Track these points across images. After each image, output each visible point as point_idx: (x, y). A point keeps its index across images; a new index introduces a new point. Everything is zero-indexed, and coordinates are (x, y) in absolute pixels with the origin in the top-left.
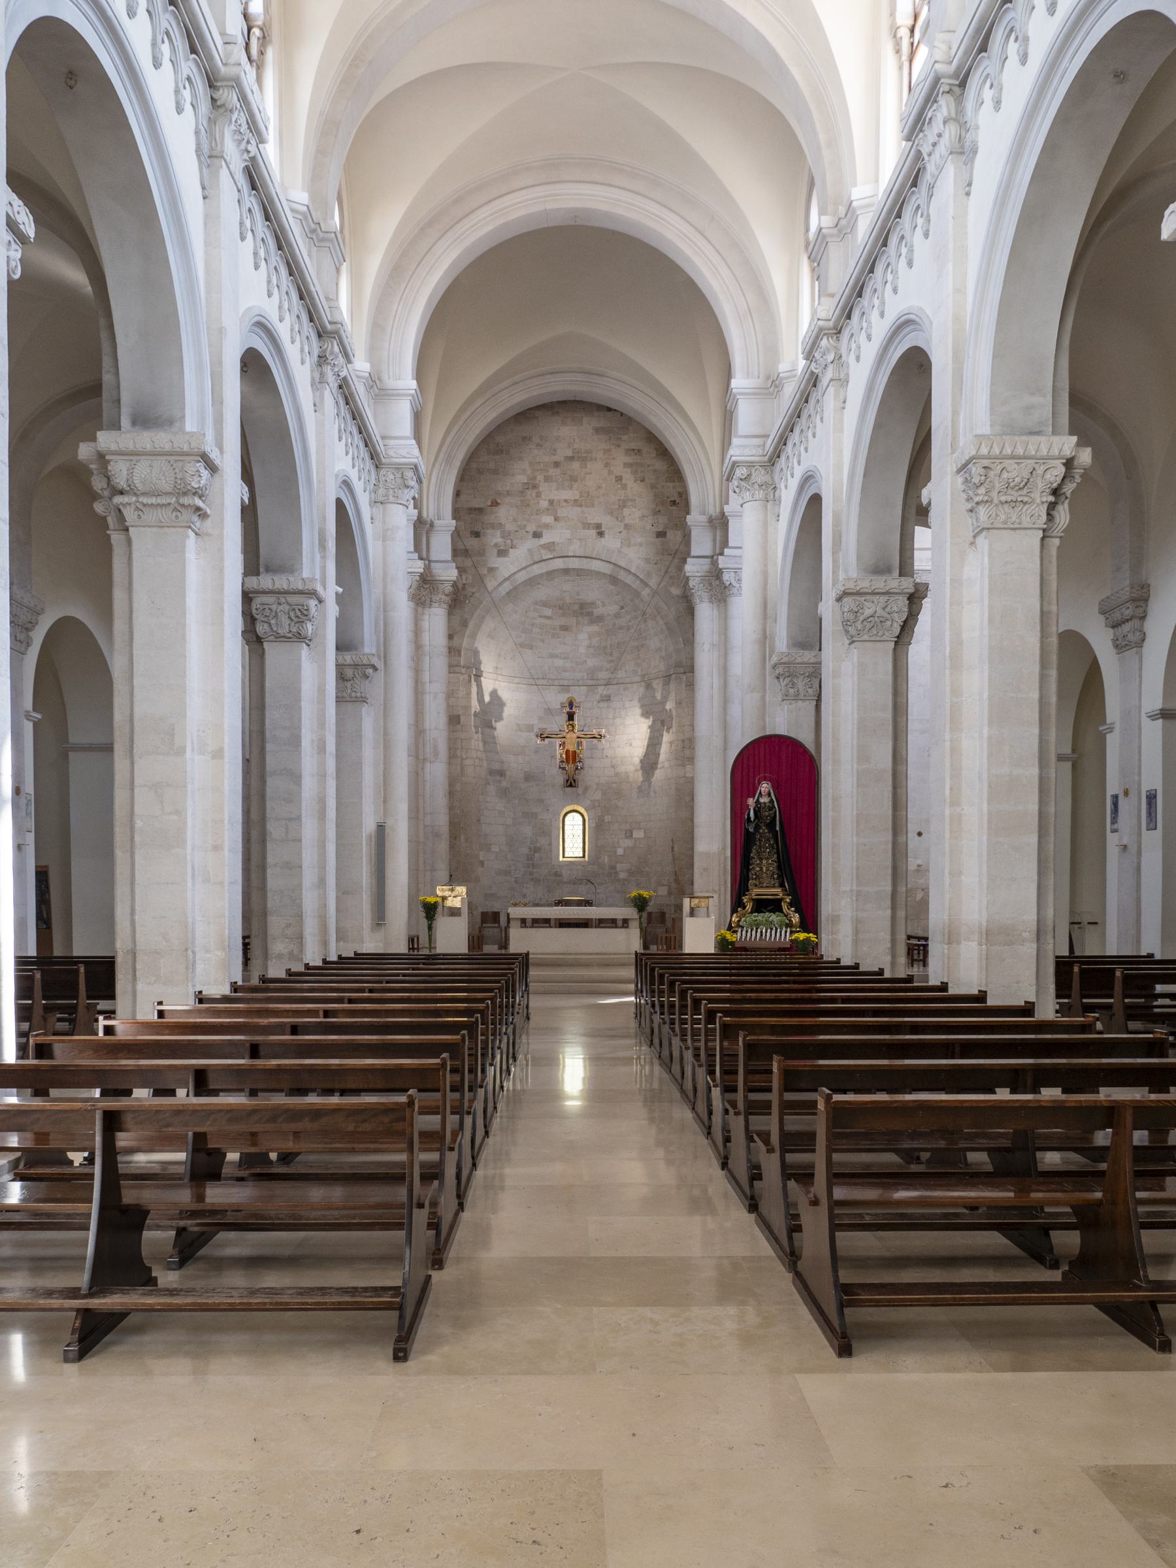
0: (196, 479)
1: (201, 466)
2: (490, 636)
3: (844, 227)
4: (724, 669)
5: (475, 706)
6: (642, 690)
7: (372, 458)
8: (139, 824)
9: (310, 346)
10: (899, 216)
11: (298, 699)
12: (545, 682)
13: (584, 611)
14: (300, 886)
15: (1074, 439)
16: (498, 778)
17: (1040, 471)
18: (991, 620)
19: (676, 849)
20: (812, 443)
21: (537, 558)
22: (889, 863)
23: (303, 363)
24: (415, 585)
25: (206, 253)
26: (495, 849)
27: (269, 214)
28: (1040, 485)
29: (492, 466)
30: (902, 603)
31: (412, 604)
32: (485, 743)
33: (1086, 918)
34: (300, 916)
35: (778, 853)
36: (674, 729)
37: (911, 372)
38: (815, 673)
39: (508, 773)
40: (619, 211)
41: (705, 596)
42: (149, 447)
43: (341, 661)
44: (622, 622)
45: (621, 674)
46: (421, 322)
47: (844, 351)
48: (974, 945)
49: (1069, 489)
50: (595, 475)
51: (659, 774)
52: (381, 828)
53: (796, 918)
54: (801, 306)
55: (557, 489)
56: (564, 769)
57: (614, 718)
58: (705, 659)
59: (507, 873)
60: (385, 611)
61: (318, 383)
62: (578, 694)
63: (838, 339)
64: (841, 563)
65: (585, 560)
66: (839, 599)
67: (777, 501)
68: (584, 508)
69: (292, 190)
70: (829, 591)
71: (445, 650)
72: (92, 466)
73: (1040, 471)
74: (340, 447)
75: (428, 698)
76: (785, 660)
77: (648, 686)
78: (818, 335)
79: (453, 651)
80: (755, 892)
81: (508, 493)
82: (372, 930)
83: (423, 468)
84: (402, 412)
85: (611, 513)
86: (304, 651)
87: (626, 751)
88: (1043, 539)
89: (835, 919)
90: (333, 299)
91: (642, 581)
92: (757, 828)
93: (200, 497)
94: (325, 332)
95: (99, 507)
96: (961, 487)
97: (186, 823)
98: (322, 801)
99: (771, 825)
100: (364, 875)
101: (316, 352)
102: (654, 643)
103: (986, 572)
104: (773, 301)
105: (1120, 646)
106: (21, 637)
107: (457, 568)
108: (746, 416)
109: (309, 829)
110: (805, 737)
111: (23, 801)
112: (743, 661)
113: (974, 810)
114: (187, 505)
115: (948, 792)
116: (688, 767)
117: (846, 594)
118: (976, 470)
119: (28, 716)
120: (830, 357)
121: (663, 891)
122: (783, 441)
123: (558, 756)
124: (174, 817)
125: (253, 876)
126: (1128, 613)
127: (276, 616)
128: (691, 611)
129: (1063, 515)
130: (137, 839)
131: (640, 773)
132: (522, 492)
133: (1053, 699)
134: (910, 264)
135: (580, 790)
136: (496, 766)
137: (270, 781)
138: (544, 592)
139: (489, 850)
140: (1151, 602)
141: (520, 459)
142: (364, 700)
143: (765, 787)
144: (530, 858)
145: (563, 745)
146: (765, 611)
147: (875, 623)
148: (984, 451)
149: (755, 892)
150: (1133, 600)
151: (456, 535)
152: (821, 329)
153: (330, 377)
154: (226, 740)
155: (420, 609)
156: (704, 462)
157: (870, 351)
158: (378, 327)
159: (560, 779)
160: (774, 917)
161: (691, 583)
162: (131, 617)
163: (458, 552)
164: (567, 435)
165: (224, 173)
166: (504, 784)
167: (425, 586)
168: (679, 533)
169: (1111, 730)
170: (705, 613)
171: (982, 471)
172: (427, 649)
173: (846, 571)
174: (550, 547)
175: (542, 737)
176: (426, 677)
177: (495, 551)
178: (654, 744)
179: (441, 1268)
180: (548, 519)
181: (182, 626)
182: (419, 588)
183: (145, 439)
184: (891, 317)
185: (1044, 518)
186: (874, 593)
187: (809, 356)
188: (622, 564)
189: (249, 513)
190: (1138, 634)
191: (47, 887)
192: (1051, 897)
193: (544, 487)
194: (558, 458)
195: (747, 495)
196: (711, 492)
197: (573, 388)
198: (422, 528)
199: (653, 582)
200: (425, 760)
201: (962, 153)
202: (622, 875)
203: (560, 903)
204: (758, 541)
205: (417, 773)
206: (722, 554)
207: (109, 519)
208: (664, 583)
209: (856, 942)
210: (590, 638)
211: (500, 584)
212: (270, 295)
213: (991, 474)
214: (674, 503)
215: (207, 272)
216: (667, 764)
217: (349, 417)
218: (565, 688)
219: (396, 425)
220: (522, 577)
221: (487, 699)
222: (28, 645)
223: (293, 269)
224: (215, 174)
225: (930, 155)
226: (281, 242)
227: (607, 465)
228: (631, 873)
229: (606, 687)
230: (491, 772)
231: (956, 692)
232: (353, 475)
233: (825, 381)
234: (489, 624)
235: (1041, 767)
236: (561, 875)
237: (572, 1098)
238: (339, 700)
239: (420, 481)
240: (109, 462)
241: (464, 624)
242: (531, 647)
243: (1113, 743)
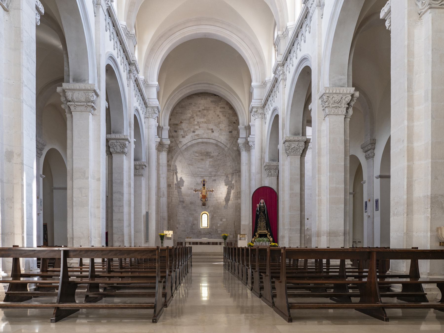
0: (92, 98)
1: (94, 94)
3: (285, 35)
4: (250, 171)
5: (175, 182)
6: (225, 178)
7: (146, 101)
8: (74, 199)
9: (126, 67)
10: (301, 28)
11: (123, 171)
12: (196, 175)
13: (208, 154)
14: (123, 226)
15: (354, 88)
17: (344, 98)
18: (330, 141)
20: (276, 99)
22: (299, 220)
23: (124, 72)
24: (157, 145)
25: (96, 32)
26: (181, 224)
27: (114, 25)
28: (344, 102)
29: (180, 112)
30: (303, 144)
31: (156, 151)
32: (178, 193)
33: (357, 241)
34: (123, 235)
36: (235, 189)
37: (306, 74)
38: (277, 169)
40: (219, 34)
41: (244, 149)
42: (78, 88)
43: (135, 164)
44: (219, 158)
45: (219, 173)
46: (160, 65)
47: (285, 71)
48: (325, 237)
49: (352, 104)
50: (211, 114)
51: (230, 202)
52: (147, 213)
53: (271, 239)
54: (272, 59)
58: (244, 168)
59: (185, 231)
61: (129, 78)
62: (206, 179)
63: (283, 67)
64: (285, 132)
66: (284, 143)
67: (265, 118)
69: (122, 22)
70: (281, 141)
71: (166, 165)
72: (61, 94)
73: (344, 98)
74: (135, 99)
75: (161, 179)
76: (268, 164)
77: (227, 177)
78: (278, 66)
79: (169, 166)
80: (259, 232)
81: (185, 120)
83: (160, 108)
84: (154, 92)
85: (216, 126)
86: (125, 157)
87: (221, 196)
88: (345, 118)
89: (283, 237)
90: (133, 54)
92: (260, 213)
93: (94, 103)
94: (131, 63)
95: (63, 106)
96: (320, 103)
97: (89, 199)
98: (130, 201)
100: (142, 227)
101: (128, 69)
102: (229, 164)
103: (328, 127)
104: (264, 59)
105: (367, 158)
106: (39, 152)
108: (256, 93)
109: (126, 209)
110: (274, 187)
111: (39, 202)
112: (255, 168)
113: (325, 197)
114: (90, 106)
115: (317, 192)
116: (239, 200)
117: (286, 141)
118: (325, 97)
119: (41, 176)
120: (281, 72)
122: (267, 100)
124: (85, 198)
125: (109, 223)
126: (369, 148)
127: (116, 146)
128: (239, 154)
129: (351, 111)
130: (74, 204)
133: (348, 165)
134: (305, 42)
135: (207, 207)
136: (182, 200)
137: (114, 195)
138: (196, 149)
139: (179, 224)
140: (376, 144)
141: (189, 109)
142: (142, 175)
143: (262, 201)
144: (192, 227)
146: (262, 150)
147: (295, 150)
148: (327, 92)
149: (259, 232)
150: (371, 144)
151: (170, 131)
152: (278, 64)
153: (132, 77)
154: (101, 175)
156: (244, 111)
157: (293, 69)
158: (146, 66)
159: (201, 203)
160: (265, 239)
161: (240, 146)
162: (72, 138)
164: (203, 102)
165: (101, 9)
166: (184, 205)
167: (160, 146)
168: (236, 132)
169: (365, 183)
170: (244, 154)
171: (327, 98)
172: (161, 164)
173: (286, 135)
174: (198, 135)
175: (195, 191)
176: (161, 172)
178: (229, 193)
179: (166, 307)
180: (197, 127)
181: (88, 141)
182: (159, 146)
183: (77, 86)
184: (299, 58)
185: (345, 112)
186: (294, 141)
187: (275, 73)
188: (219, 140)
189: (108, 111)
190: (372, 154)
191: (47, 229)
192: (348, 224)
193: (196, 118)
194: (200, 109)
195: (256, 117)
196: (245, 119)
197: (204, 88)
198: (160, 129)
199: (228, 146)
200: (160, 197)
201: (320, 6)
202: (219, 232)
204: (260, 130)
206: (249, 137)
207: (66, 110)
209: (289, 243)
211: (183, 146)
212: (114, 49)
213: (330, 98)
214: (234, 123)
215: (96, 38)
217: (138, 91)
218: (202, 177)
219: (152, 95)
220: (189, 144)
221: (179, 180)
222: (41, 155)
223: (121, 43)
224: (98, 10)
225: (310, 7)
226: (118, 34)
227: (214, 111)
229: (214, 177)
230: (180, 201)
231: (319, 163)
232: (139, 108)
233: (279, 80)
234: (179, 158)
235: (345, 185)
237: (205, 286)
238: (135, 175)
239: (159, 112)
240: (66, 92)
241: (172, 158)
243: (365, 186)
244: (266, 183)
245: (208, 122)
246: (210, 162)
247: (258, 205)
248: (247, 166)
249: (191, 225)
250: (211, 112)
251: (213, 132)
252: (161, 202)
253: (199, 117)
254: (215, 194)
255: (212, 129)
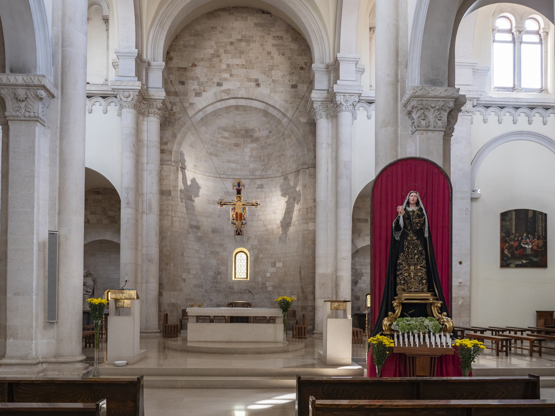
2: (191, 146)
5: (181, 186)
12: (224, 176)
13: (247, 134)
16: (195, 230)
19: (302, 273)
21: (219, 99)
26: (193, 272)
29: (192, 43)
32: (187, 208)
35: (427, 258)
36: (301, 202)
39: (202, 228)
41: (324, 114)
44: (270, 141)
45: (269, 172)
50: (255, 50)
51: (292, 229)
52: (54, 238)
55: (232, 58)
56: (234, 224)
57: (265, 198)
59: (200, 286)
60: (63, 46)
65: (249, 101)
68: (249, 70)
76: (420, 93)
77: (286, 178)
81: (202, 59)
82: (45, 328)
85: (264, 73)
91: (283, 114)
99: (419, 233)
102: (289, 152)
107: (165, 91)
121: (294, 298)
123: (231, 216)
128: (312, 125)
131: (280, 229)
132: (211, 59)
136: (194, 223)
138: (224, 121)
139: (189, 273)
141: (210, 39)
142: (36, 120)
143: (413, 196)
144: (215, 278)
145: (234, 209)
155: (141, 118)
159: (231, 229)
163: (166, 82)
166: (199, 234)
170: (324, 126)
172: (146, 142)
174: (227, 91)
175: (221, 204)
176: (145, 160)
177: (194, 94)
178: (289, 212)
180: (226, 75)
193: (223, 56)
196: (327, 46)
199: (289, 114)
200: (143, 213)
202: (270, 289)
203: (231, 305)
205: (137, 220)
206: (336, 83)
208: (295, 115)
210: (251, 151)
214: (302, 68)
216: (297, 223)
220: (210, 109)
221: (189, 183)
227: (262, 45)
228: (275, 287)
230: (192, 227)
234: (190, 138)
236: (233, 288)
242: (216, 156)
244: (413, 148)
245: (248, 65)
246: (252, 150)
247: (400, 209)
248: (330, 150)
249: (213, 274)
250: (255, 46)
251: (258, 85)
252: (145, 223)
253: (230, 55)
254: (261, 213)
255: (257, 80)
